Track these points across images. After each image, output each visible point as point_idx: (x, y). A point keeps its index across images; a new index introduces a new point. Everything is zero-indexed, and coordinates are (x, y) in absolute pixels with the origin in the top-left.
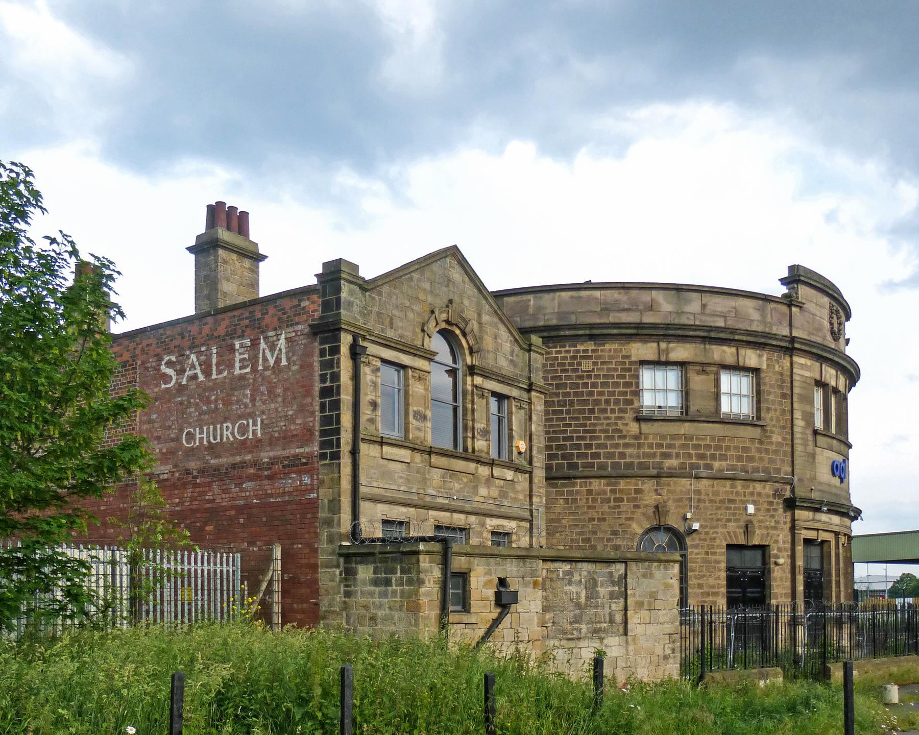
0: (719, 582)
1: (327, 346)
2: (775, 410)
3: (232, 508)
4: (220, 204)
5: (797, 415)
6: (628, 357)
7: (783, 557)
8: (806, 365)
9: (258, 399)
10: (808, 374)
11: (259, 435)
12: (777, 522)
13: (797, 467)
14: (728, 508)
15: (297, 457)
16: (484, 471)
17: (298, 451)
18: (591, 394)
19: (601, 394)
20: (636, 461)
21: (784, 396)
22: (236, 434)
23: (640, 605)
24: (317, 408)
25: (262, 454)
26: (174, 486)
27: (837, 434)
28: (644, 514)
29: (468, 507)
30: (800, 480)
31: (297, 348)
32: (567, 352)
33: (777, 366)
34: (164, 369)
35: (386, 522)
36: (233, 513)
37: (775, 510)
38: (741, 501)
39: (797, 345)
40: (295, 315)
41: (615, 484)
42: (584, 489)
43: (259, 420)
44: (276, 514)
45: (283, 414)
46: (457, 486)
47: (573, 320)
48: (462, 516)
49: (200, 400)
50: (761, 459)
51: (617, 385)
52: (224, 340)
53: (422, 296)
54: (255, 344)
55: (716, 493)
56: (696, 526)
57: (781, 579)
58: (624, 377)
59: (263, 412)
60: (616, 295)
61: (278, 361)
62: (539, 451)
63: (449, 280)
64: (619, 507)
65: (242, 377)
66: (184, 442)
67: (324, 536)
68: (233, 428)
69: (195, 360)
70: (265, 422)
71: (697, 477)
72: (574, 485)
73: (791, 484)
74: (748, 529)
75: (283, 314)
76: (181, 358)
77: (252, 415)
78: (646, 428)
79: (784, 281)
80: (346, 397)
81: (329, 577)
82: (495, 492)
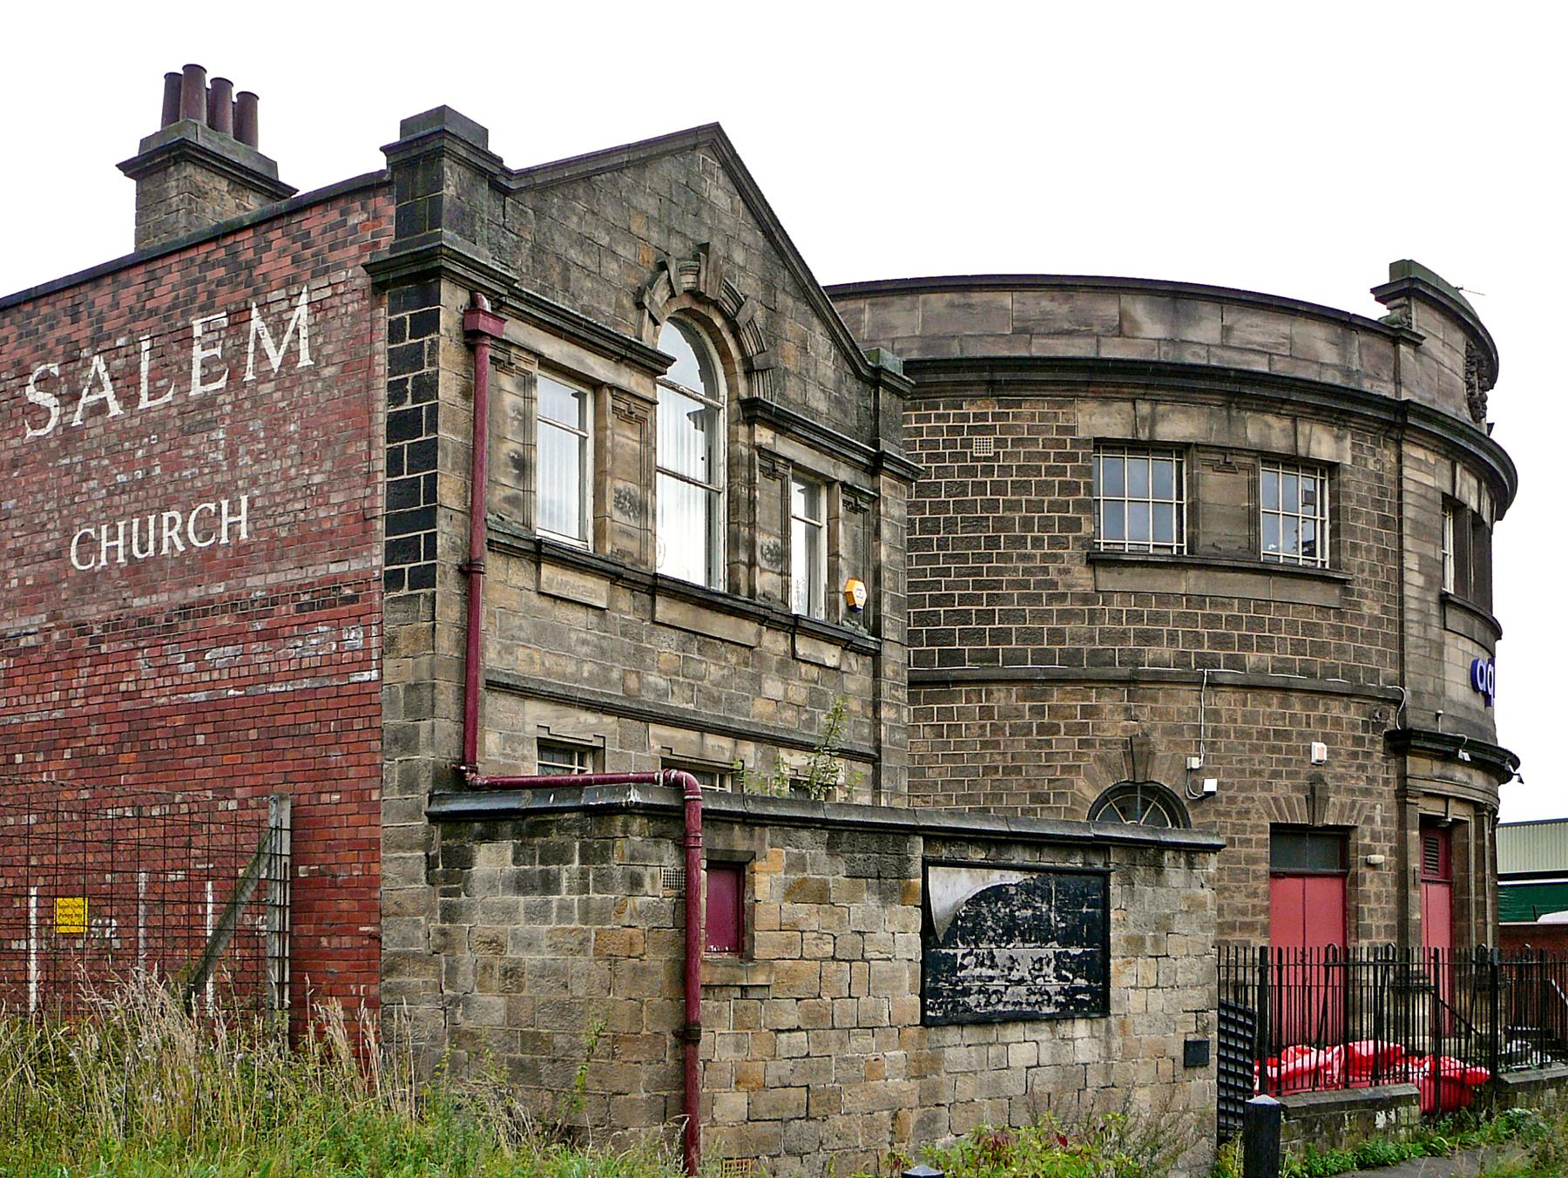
0: (1256, 901)
1: (406, 315)
2: (1369, 550)
3: (177, 709)
4: (195, 71)
5: (1411, 562)
6: (1070, 430)
7: (1383, 852)
8: (1426, 463)
9: (242, 450)
10: (1429, 481)
11: (244, 536)
12: (1370, 780)
13: (1409, 668)
14: (1274, 749)
15: (335, 583)
16: (776, 643)
17: (333, 568)
18: (992, 506)
19: (1012, 506)
20: (1086, 647)
21: (1384, 522)
22: (191, 535)
23: (1136, 944)
24: (381, 464)
25: (250, 582)
26: (49, 664)
27: (1472, 605)
28: (1101, 759)
29: (738, 721)
30: (1417, 694)
31: (337, 323)
32: (939, 417)
33: (1371, 461)
34: (33, 394)
35: (547, 746)
36: (180, 721)
37: (1368, 755)
38: (1300, 734)
39: (1411, 420)
40: (332, 248)
41: (1044, 695)
42: (975, 705)
43: (244, 499)
44: (279, 720)
45: (299, 483)
46: (715, 672)
47: (955, 351)
48: (726, 743)
49: (114, 462)
50: (1341, 650)
51: (1044, 488)
52: (166, 319)
53: (637, 226)
54: (239, 318)
55: (1250, 718)
56: (1210, 785)
57: (1378, 897)
58: (1063, 472)
59: (254, 481)
60: (1045, 303)
61: (291, 355)
62: (897, 605)
63: (702, 200)
64: (1049, 743)
65: (207, 402)
66: (74, 561)
67: (392, 770)
68: (185, 523)
69: (102, 368)
70: (259, 503)
71: (1213, 685)
72: (952, 698)
73: (1398, 703)
74: (1315, 793)
75: (305, 247)
76: (71, 367)
77: (223, 491)
78: (1108, 580)
79: (1381, 294)
80: (450, 436)
81: (402, 874)
82: (799, 693)
